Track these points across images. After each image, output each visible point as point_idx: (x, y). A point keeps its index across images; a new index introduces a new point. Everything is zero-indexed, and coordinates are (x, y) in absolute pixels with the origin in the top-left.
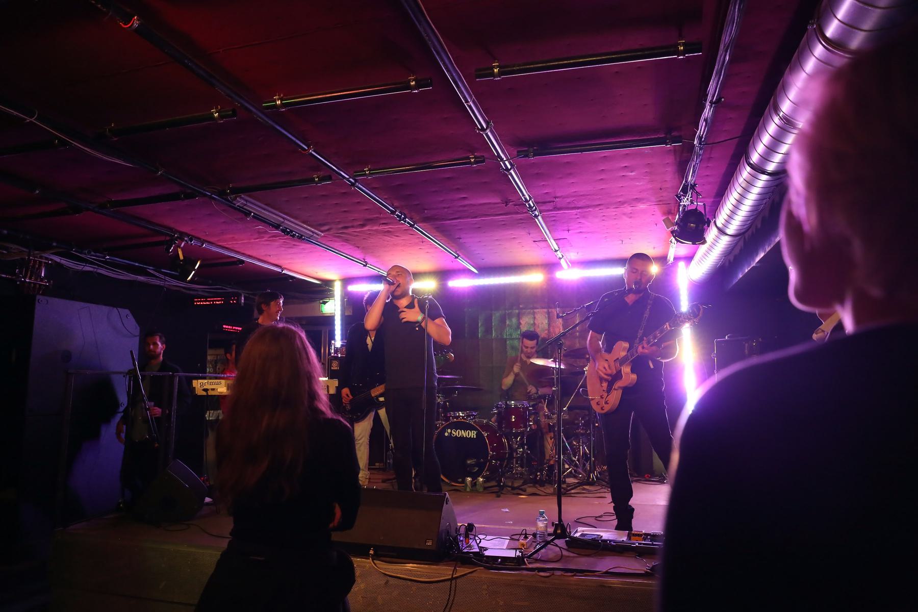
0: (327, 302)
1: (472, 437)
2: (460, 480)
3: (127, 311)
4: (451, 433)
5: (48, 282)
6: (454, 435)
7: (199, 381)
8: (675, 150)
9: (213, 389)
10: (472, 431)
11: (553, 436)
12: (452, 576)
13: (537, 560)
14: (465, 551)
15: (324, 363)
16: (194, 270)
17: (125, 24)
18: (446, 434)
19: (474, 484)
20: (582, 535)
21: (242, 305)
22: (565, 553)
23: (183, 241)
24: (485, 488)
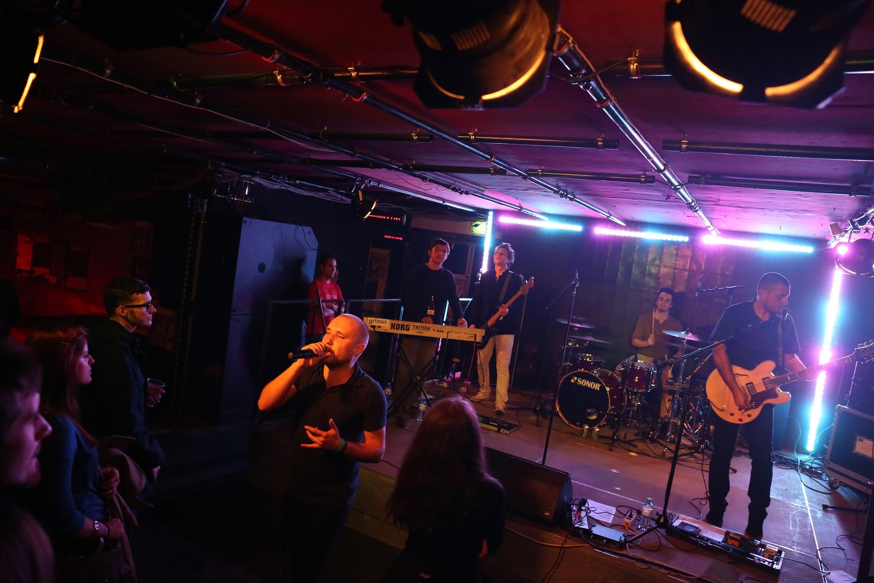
0: (478, 225)
1: (596, 389)
2: (578, 424)
3: (309, 229)
4: (577, 381)
5: (251, 200)
6: (579, 383)
7: (369, 318)
8: (852, 275)
9: (379, 327)
10: (597, 384)
11: (671, 399)
12: (562, 545)
13: (639, 547)
14: (576, 525)
15: (467, 275)
16: (371, 210)
17: (356, 99)
18: (572, 381)
19: (591, 431)
20: (682, 523)
21: (404, 224)
22: (664, 542)
23: (363, 184)
24: (600, 437)
